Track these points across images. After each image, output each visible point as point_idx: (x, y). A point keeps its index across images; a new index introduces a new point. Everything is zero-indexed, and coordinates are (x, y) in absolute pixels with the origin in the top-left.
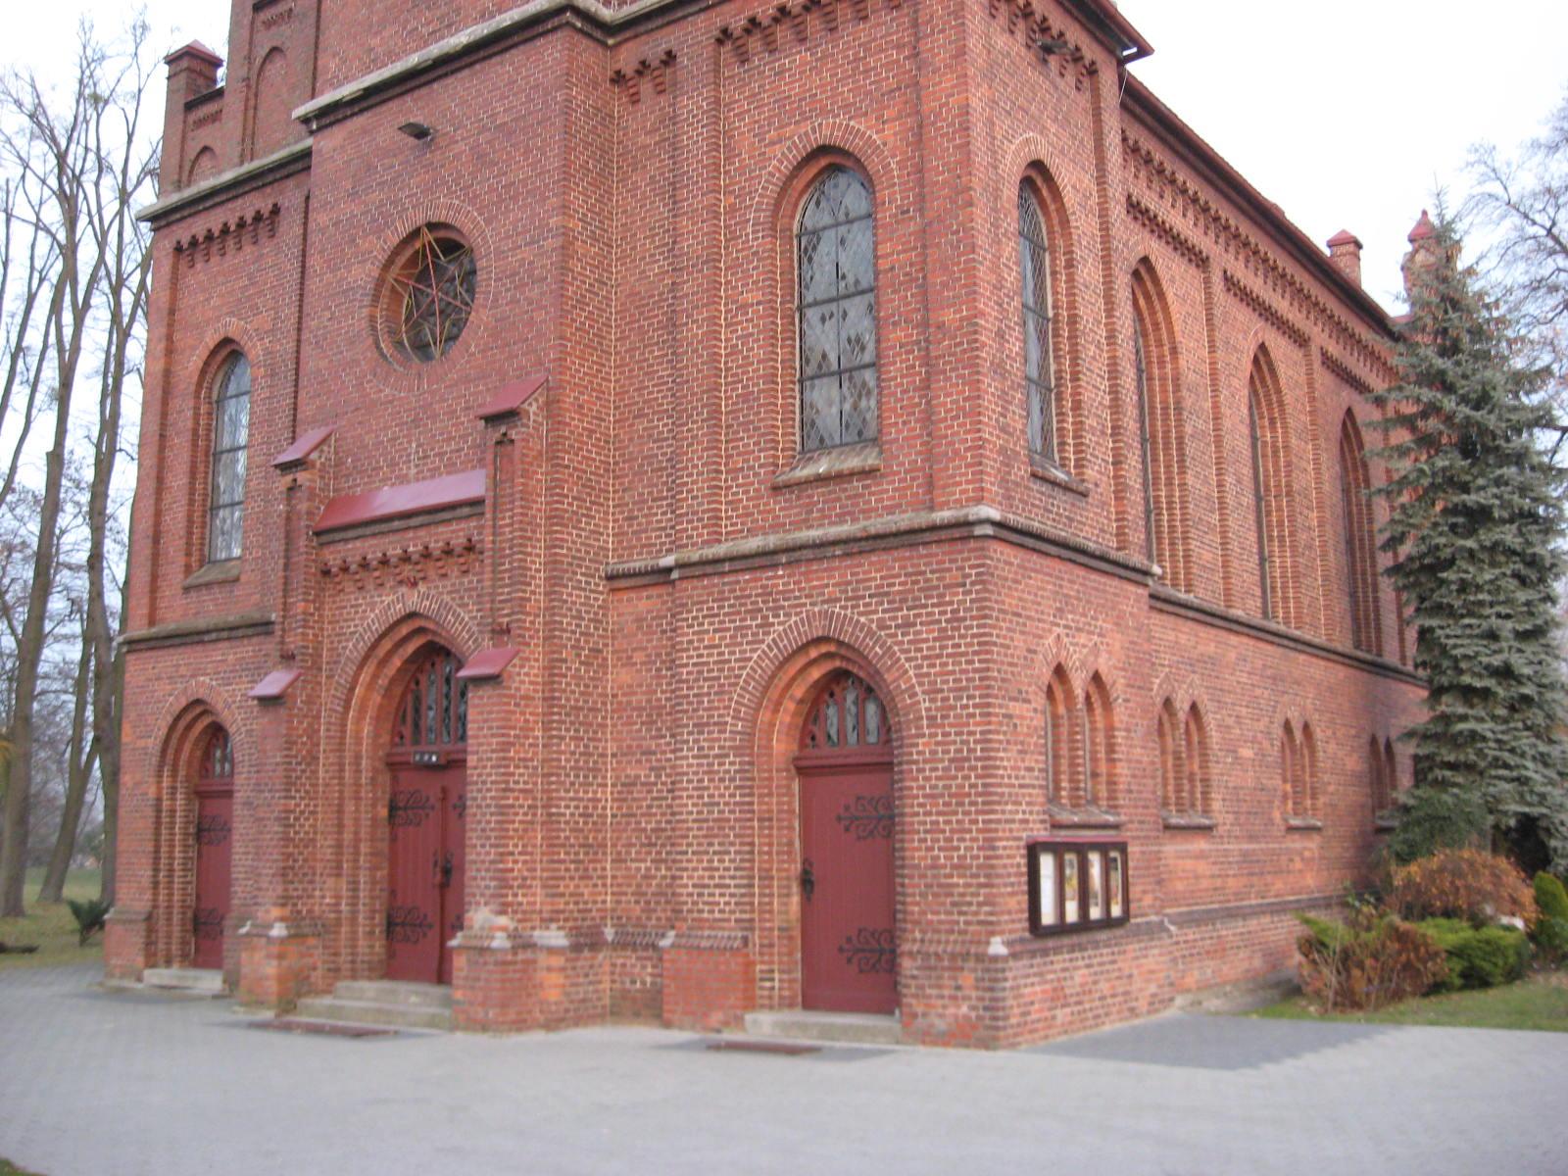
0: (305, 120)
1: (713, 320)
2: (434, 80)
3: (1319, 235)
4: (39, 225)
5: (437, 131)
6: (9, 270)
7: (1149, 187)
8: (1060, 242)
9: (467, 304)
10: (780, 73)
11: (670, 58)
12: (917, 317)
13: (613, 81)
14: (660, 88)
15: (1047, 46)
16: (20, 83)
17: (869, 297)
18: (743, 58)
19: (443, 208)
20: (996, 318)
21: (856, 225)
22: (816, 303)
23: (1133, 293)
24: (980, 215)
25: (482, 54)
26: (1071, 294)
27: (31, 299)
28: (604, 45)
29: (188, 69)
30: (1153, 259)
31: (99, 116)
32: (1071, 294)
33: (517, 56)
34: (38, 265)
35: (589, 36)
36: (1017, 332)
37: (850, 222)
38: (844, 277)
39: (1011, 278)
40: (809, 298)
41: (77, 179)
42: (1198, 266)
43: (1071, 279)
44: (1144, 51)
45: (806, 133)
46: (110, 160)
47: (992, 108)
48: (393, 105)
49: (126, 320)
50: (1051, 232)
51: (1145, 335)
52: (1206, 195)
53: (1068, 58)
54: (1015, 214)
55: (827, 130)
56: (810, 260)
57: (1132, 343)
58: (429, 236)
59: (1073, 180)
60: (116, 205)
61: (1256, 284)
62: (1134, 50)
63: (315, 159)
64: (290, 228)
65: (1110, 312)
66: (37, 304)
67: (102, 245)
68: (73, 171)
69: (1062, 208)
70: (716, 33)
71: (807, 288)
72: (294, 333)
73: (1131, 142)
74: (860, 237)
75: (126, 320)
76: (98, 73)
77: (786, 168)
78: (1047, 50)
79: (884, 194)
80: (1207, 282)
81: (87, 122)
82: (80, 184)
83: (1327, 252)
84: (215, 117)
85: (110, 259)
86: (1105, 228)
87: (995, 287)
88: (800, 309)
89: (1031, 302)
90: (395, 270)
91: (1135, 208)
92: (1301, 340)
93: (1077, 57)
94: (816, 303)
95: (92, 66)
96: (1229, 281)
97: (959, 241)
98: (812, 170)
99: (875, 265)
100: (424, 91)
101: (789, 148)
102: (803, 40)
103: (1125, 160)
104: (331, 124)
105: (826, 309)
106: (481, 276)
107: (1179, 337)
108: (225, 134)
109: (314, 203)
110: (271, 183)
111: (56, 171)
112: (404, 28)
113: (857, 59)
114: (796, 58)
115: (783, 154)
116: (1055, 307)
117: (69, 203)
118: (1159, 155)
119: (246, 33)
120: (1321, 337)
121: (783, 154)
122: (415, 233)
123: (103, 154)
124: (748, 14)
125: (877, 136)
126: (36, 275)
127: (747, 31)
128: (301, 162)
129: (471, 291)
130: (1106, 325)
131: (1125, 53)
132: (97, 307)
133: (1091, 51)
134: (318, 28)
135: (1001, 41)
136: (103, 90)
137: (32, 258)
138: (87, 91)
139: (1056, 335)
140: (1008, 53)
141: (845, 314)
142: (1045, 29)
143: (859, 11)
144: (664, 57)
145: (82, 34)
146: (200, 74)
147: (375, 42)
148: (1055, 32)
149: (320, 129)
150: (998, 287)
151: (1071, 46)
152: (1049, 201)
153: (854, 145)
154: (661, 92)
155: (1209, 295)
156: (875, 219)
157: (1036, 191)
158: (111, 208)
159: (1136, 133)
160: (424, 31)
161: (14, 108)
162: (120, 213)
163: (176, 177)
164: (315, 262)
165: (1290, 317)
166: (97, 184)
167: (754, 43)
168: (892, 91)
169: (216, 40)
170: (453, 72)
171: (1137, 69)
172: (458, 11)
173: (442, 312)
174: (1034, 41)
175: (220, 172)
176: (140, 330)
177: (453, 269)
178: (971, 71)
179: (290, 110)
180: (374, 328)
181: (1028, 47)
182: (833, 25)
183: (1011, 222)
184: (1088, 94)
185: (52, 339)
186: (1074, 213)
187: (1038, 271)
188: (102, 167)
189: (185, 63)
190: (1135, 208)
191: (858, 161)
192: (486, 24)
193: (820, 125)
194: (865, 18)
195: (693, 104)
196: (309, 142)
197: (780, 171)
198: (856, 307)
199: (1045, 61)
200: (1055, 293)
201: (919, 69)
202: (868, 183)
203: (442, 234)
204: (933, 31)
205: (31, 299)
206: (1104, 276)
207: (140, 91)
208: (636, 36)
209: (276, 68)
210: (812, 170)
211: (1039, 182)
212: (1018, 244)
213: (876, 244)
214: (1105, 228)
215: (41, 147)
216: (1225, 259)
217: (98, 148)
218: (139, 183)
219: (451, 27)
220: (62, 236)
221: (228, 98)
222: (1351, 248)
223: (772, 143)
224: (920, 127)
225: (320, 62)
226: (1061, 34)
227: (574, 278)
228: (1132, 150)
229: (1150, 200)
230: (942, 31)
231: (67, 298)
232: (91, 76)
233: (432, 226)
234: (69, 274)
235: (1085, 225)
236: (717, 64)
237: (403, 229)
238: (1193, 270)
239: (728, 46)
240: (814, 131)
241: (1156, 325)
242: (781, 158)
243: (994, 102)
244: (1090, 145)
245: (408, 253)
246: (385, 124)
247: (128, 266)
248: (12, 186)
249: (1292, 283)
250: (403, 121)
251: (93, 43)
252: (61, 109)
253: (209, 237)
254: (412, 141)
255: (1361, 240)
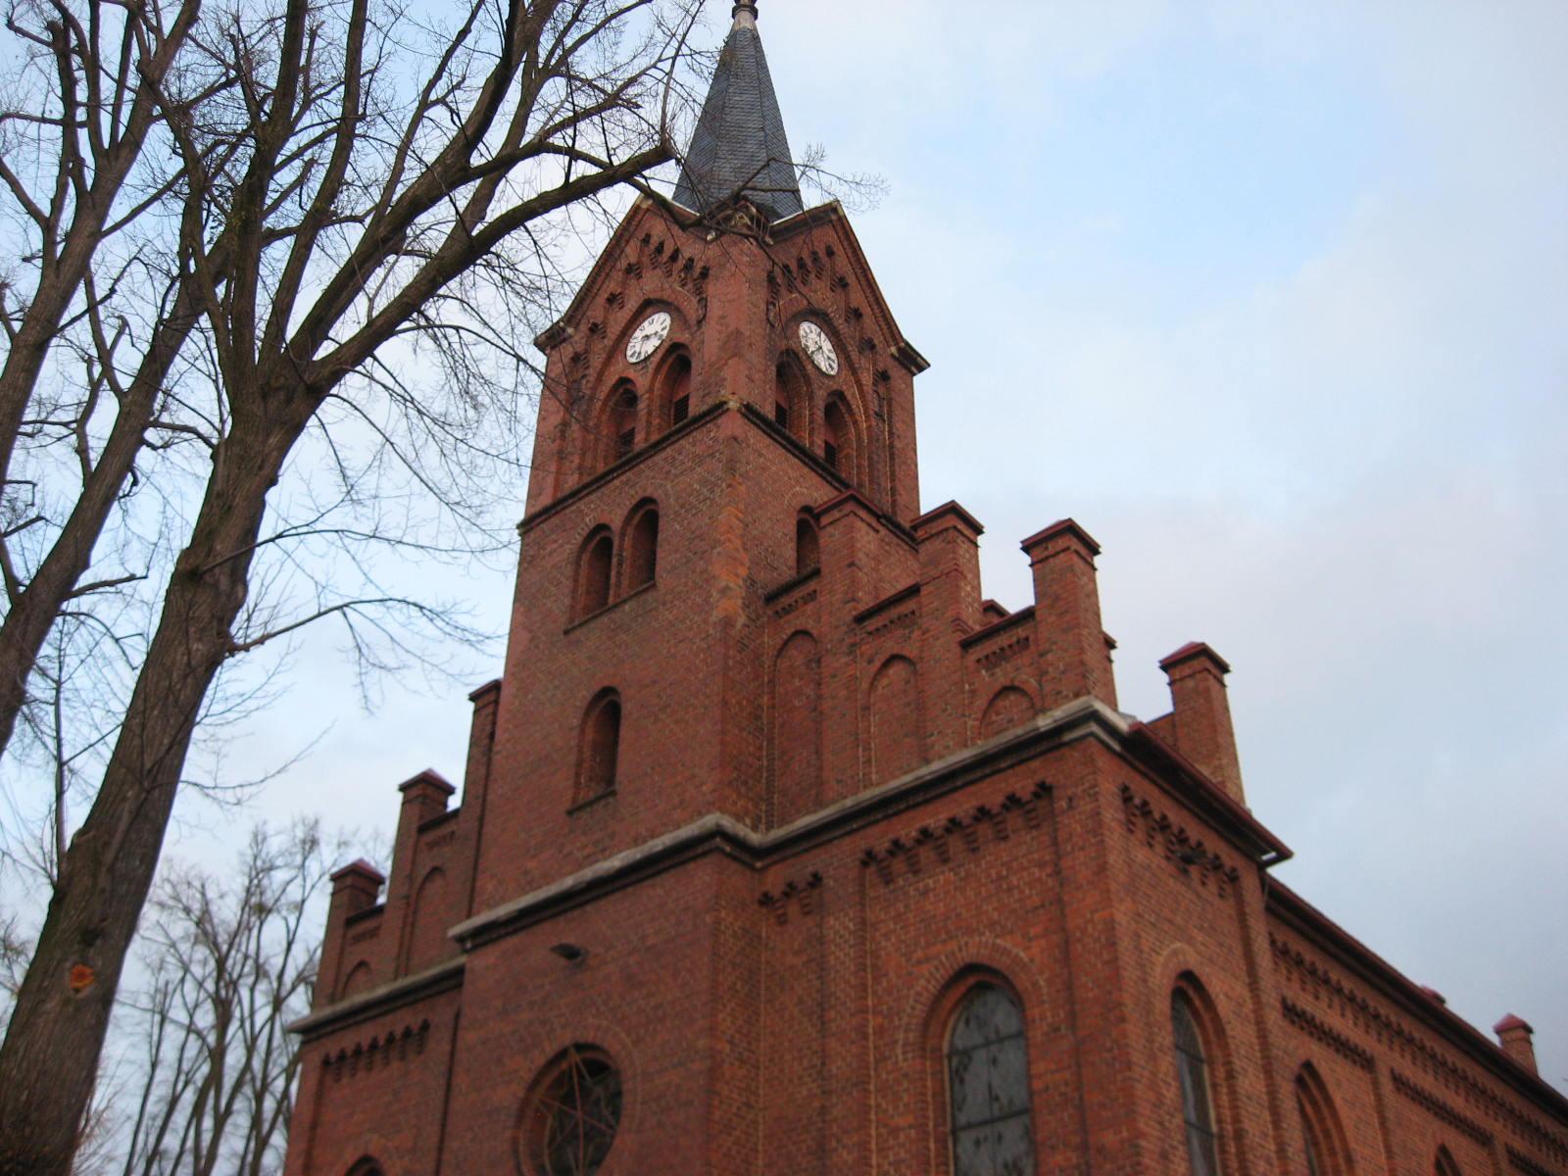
0: (461, 939)
1: (864, 1146)
2: (587, 902)
3: (1483, 1019)
4: (191, 1029)
5: (587, 952)
6: (317, 620)
7: (1304, 989)
8: (1218, 1053)
9: (611, 1127)
10: (925, 893)
11: (816, 880)
12: (1076, 1139)
13: (761, 903)
14: (806, 910)
15: (1187, 858)
16: (192, 892)
17: (1025, 1119)
18: (888, 880)
19: (593, 1028)
20: (1159, 1139)
21: (1006, 1043)
22: (969, 1126)
23: (1299, 1101)
24: (1134, 1030)
25: (634, 877)
26: (1234, 1108)
27: (173, 1102)
28: (752, 868)
29: (352, 886)
30: (1315, 1062)
31: (261, 924)
32: (1234, 1108)
33: (668, 880)
34: (186, 1066)
35: (735, 858)
36: (1181, 1151)
37: (1000, 1040)
38: (997, 1098)
39: (1170, 1094)
40: (962, 1119)
41: (234, 985)
42: (1362, 1066)
43: (1233, 1092)
44: (1284, 854)
45: (953, 953)
46: (267, 967)
47: (1137, 922)
48: (548, 926)
49: (266, 1126)
50: (1207, 1042)
51: (1316, 1144)
52: (1362, 992)
53: (1209, 867)
54: (1169, 1026)
55: (975, 948)
56: (962, 1081)
57: (1303, 1155)
58: (575, 1058)
59: (1225, 988)
60: (267, 1011)
61: (1427, 1081)
62: (1273, 854)
63: (467, 978)
64: (438, 1045)
65: (1277, 1123)
66: (179, 1107)
67: (250, 1049)
68: (230, 975)
69: (1216, 1018)
70: (861, 855)
71: (960, 1109)
72: (779, 187)
73: (1279, 944)
74: (1012, 1056)
75: (266, 1126)
76: (265, 882)
77: (933, 987)
78: (1187, 860)
79: (1034, 1012)
80: (1375, 1084)
81: (250, 930)
82: (235, 990)
83: (1495, 1039)
84: (373, 933)
85: (257, 1064)
86: (1263, 1036)
87: (1154, 1105)
88: (954, 1132)
89: (1193, 1117)
90: (541, 1090)
91: (1290, 1011)
92: (1483, 1139)
93: (1217, 866)
94: (969, 1126)
95: (261, 876)
96: (1399, 1081)
97: (1114, 1058)
98: (961, 989)
99: (1029, 1085)
100: (576, 913)
101: (937, 968)
102: (945, 861)
103: (1276, 963)
104: (486, 944)
105: (981, 1133)
106: (627, 1099)
107: (1353, 1145)
108: (382, 950)
109: (464, 1022)
110: (423, 999)
111: (215, 974)
112: (560, 852)
113: (1000, 878)
114: (941, 878)
115: (931, 974)
116: (1219, 1121)
117: (223, 1010)
118: (1309, 955)
119: (409, 853)
120: (1502, 1133)
121: (931, 974)
122: (562, 1054)
123: (261, 960)
124: (892, 836)
125: (1025, 953)
126: (183, 1078)
127: (891, 853)
128: (455, 978)
129: (616, 1112)
130: (1274, 1138)
131: (1265, 858)
132: (239, 1112)
133: (1230, 858)
134: (478, 849)
135: (1141, 855)
136: (269, 898)
137: (180, 1060)
138: (254, 900)
139: (1223, 1151)
140: (1149, 866)
141: (1000, 1138)
142: (1183, 839)
143: (999, 831)
144: (810, 879)
145: (254, 845)
146: (363, 890)
147: (531, 865)
148: (1193, 842)
149: (475, 947)
150: (1158, 1104)
151: (1210, 855)
152: (1202, 1011)
153: (1001, 963)
154: (808, 913)
155: (1379, 1097)
156: (1027, 1039)
157: (1189, 1002)
158: (263, 1014)
159: (1284, 936)
160: (579, 855)
161: (182, 915)
162: (272, 1019)
163: (330, 990)
164: (461, 1081)
165: (1468, 1114)
166: (252, 990)
167: (899, 865)
168: (1037, 908)
169: (381, 858)
170: (606, 894)
171: (1278, 872)
172: (612, 836)
173: (586, 1135)
174: (1172, 852)
175: (374, 987)
176: (278, 1139)
177: (598, 1091)
178: (1113, 887)
179: (445, 929)
180: (515, 1151)
181: (1168, 858)
182: (976, 845)
183: (1165, 1037)
184: (1232, 901)
185: (190, 1143)
186: (1229, 1022)
187: (1198, 1085)
188: (260, 972)
189: (349, 881)
190: (1290, 1011)
191: (1005, 979)
192: (639, 848)
193: (966, 943)
194: (1005, 838)
195: (839, 925)
196: (462, 959)
197: (927, 990)
198: (1012, 1130)
199: (1185, 872)
200: (1218, 1106)
201: (1061, 885)
202: (1017, 1001)
203: (589, 1055)
204: (1073, 847)
205: (173, 1102)
206: (1267, 1086)
207: (303, 901)
208: (783, 859)
209: (436, 886)
210: (961, 989)
211: (1191, 993)
212: (1173, 1057)
213: (1029, 1063)
214: (1263, 1036)
215: (202, 952)
216: (1391, 1059)
217: (258, 954)
218: (294, 988)
219: (605, 852)
220: (211, 1039)
221: (386, 916)
222: (1521, 1033)
223: (919, 962)
224: (1067, 942)
225: (478, 884)
226: (1200, 844)
227: (721, 1102)
228: (1281, 952)
229: (1305, 1002)
230: (1082, 849)
231: (211, 1102)
232: (258, 886)
233: (579, 1047)
234: (215, 1078)
235: (1241, 1034)
236: (862, 885)
237: (551, 1049)
238: (1358, 1072)
239: (873, 868)
240: (960, 950)
241: (1327, 1134)
242: (928, 980)
243: (1139, 915)
244: (1238, 950)
245: (554, 1073)
246: (537, 946)
247: (274, 1071)
248: (171, 987)
249: (1465, 1078)
250: (555, 942)
251: (263, 855)
252: (227, 912)
253: (358, 1052)
254: (562, 962)
255: (1531, 1023)
